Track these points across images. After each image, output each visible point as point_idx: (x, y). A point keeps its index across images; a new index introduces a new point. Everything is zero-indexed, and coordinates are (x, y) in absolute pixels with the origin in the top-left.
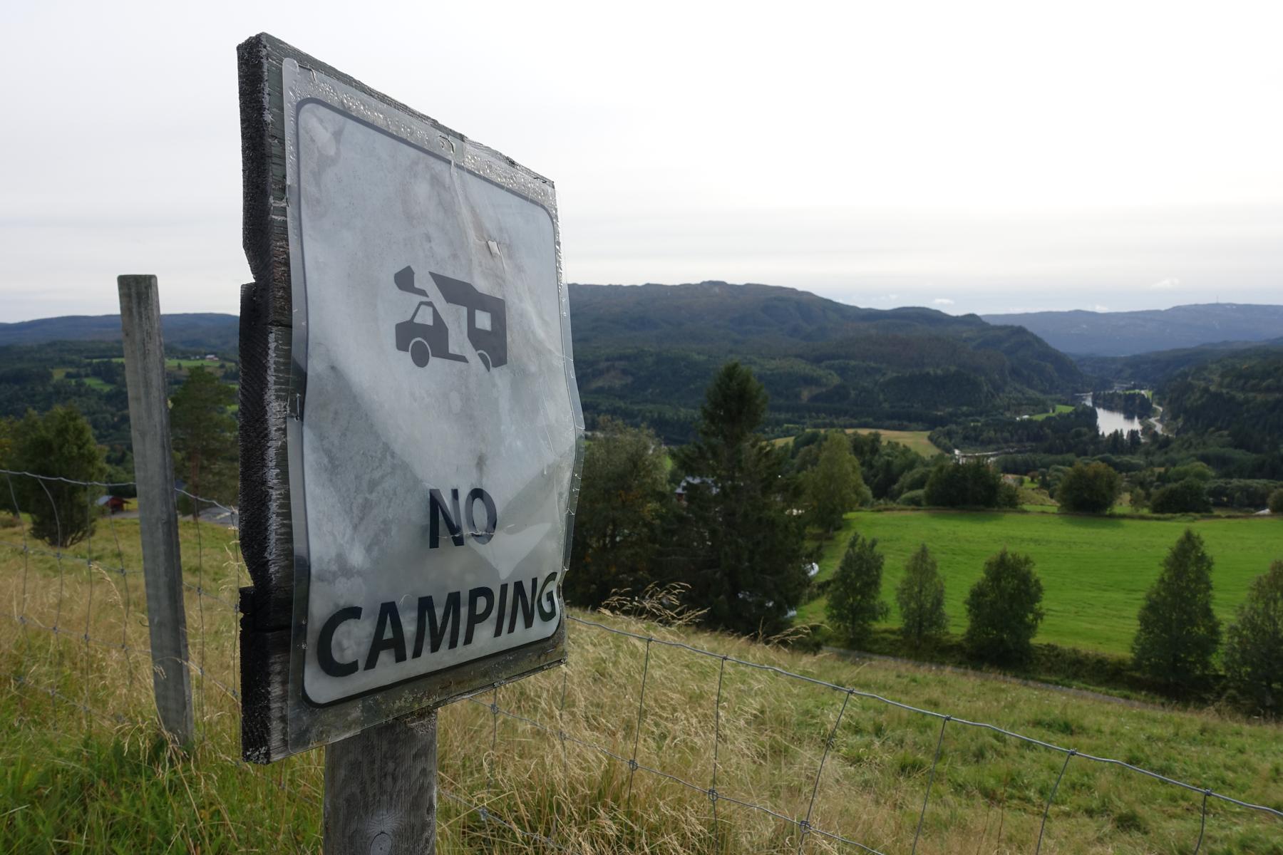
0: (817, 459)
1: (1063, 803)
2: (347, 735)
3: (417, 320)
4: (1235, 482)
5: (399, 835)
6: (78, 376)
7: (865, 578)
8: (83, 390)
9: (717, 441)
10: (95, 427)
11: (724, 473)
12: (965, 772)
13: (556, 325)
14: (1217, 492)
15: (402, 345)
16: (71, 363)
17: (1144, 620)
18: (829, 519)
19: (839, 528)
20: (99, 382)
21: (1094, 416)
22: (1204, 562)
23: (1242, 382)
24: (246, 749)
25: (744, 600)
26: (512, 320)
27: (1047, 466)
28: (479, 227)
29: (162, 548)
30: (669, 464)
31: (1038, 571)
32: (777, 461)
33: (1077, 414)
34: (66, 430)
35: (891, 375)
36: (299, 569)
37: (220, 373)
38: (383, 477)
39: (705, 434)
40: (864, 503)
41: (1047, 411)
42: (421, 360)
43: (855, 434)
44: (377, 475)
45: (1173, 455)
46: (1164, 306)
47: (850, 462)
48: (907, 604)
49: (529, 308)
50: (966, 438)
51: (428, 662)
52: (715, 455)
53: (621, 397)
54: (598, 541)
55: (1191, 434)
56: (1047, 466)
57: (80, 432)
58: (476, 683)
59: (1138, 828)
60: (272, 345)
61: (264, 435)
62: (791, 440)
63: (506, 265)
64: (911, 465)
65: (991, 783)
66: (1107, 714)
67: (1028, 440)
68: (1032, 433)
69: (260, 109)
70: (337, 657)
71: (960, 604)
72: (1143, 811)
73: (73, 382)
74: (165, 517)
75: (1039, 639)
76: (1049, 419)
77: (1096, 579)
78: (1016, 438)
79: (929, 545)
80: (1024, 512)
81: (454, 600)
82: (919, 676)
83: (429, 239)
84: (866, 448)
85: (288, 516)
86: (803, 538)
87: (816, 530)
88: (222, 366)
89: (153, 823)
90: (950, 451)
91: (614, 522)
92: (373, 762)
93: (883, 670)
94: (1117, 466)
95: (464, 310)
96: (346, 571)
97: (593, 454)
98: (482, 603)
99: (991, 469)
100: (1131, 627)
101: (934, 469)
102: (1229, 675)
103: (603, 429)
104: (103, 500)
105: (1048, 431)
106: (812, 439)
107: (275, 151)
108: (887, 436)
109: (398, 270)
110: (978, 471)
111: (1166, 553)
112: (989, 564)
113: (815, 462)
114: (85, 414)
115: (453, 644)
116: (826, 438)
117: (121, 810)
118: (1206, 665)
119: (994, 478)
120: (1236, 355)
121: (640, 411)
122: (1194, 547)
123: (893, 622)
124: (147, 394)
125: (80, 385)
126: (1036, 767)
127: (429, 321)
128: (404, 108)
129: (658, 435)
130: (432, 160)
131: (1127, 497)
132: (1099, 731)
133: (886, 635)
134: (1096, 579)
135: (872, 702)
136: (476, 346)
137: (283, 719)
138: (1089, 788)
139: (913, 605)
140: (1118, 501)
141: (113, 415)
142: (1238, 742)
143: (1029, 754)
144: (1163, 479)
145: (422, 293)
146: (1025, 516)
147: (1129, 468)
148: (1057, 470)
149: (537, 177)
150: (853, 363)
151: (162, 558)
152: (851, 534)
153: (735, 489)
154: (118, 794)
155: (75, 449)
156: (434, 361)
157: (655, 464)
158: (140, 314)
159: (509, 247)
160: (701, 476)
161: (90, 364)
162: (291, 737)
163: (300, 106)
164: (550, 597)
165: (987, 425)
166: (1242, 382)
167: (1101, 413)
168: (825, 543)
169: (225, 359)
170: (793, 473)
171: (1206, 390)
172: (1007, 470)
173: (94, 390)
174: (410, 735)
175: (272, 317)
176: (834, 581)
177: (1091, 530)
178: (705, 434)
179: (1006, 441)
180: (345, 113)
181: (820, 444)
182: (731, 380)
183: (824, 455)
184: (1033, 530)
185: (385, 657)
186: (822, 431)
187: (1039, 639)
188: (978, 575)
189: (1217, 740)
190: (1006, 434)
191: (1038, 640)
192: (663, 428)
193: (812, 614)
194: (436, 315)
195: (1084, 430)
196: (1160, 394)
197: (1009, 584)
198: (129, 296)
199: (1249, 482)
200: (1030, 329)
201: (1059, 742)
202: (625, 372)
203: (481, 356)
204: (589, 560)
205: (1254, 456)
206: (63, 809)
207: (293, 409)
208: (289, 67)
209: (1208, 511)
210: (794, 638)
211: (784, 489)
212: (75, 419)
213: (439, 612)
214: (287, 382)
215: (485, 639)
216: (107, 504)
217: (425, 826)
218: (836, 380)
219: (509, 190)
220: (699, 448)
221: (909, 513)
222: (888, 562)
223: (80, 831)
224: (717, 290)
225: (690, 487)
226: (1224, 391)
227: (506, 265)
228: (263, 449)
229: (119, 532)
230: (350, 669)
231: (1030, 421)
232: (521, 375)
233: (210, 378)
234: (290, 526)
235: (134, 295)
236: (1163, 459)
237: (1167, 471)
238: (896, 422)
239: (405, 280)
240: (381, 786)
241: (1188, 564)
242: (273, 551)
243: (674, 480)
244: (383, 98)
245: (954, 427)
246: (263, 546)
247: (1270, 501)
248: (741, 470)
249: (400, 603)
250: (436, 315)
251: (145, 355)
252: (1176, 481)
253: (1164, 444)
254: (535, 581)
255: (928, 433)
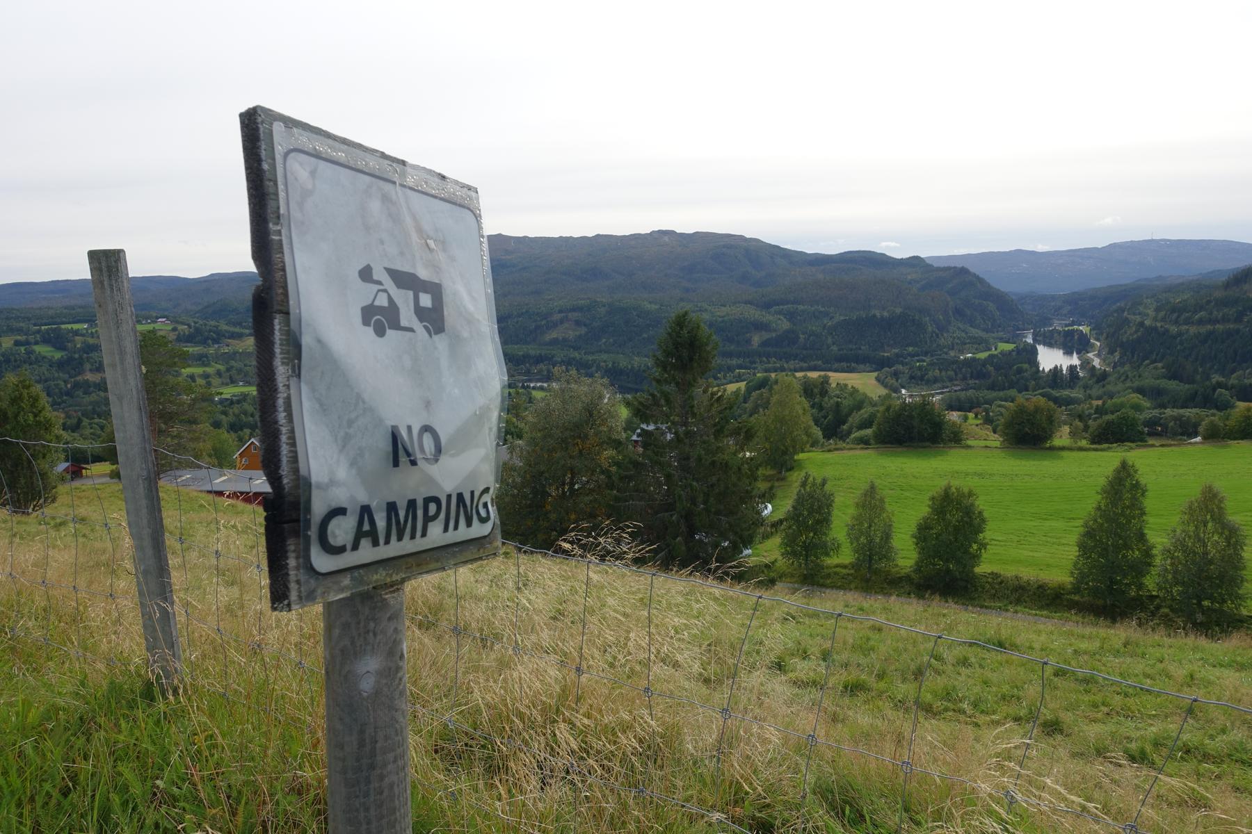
0: (768, 402)
1: (994, 713)
2: (341, 596)
3: (377, 303)
4: (1169, 412)
5: (380, 674)
6: (27, 343)
7: (817, 516)
8: (33, 357)
9: (670, 388)
10: (48, 395)
11: (677, 419)
12: (904, 689)
13: (482, 301)
14: (1152, 423)
15: (366, 322)
16: (19, 331)
17: (1082, 546)
18: (781, 460)
19: (791, 469)
20: (50, 349)
21: (1035, 352)
22: (1138, 489)
23: (1175, 315)
24: (273, 603)
25: (700, 541)
26: (447, 299)
27: (990, 402)
28: (420, 230)
29: (144, 502)
30: (624, 413)
31: (981, 504)
32: (729, 407)
33: (1018, 351)
34: (20, 398)
35: (839, 318)
36: (304, 484)
37: (172, 336)
38: (357, 417)
39: (658, 381)
40: (814, 444)
41: (990, 349)
42: (380, 332)
43: (805, 377)
44: (353, 416)
45: (1110, 388)
46: (1101, 243)
47: (800, 406)
48: (857, 539)
49: (461, 289)
50: (912, 378)
51: (396, 548)
52: (668, 401)
53: (576, 348)
54: (557, 489)
55: (1127, 367)
56: (990, 402)
57: (36, 399)
58: (432, 566)
59: (1061, 732)
60: (277, 327)
61: (274, 390)
62: (742, 385)
63: (441, 256)
64: (859, 406)
65: (928, 697)
66: (1039, 632)
67: (972, 377)
68: (976, 371)
69: (259, 161)
70: (331, 541)
71: (907, 537)
72: (1067, 717)
73: (23, 349)
74: (145, 473)
75: (983, 568)
76: (991, 356)
77: (1036, 509)
78: (960, 376)
79: (877, 482)
80: (969, 447)
81: (412, 504)
82: (866, 605)
83: (382, 242)
84: (816, 390)
85: (294, 444)
86: (756, 480)
87: (769, 472)
88: (174, 329)
89: (151, 748)
90: (897, 391)
91: (572, 470)
92: (359, 623)
93: (832, 602)
94: (1056, 400)
95: (411, 293)
96: (332, 482)
97: (548, 404)
98: (433, 508)
99: (937, 406)
100: (1071, 553)
101: (882, 409)
102: (1161, 595)
103: (558, 380)
104: (62, 466)
105: (991, 368)
106: (763, 384)
107: (271, 190)
108: (836, 378)
109: (361, 267)
110: (924, 409)
111: (1102, 481)
112: (933, 499)
113: (766, 405)
114: (38, 382)
115: (413, 537)
116: (776, 382)
117: (121, 738)
118: (1140, 586)
119: (939, 416)
120: (1170, 289)
121: (594, 361)
122: (1129, 475)
123: (846, 556)
124: (122, 361)
125: (29, 353)
126: (971, 682)
127: (385, 304)
128: (360, 146)
129: (612, 385)
130: (381, 183)
131: (1066, 429)
132: (1031, 648)
133: (838, 570)
134: (1036, 509)
135: (820, 630)
136: (421, 320)
137: (298, 582)
138: (1019, 698)
139: (863, 540)
140: (1058, 434)
141: (66, 382)
142: (1157, 653)
143: (963, 670)
144: (1100, 411)
145: (380, 283)
146: (969, 451)
147: (1069, 402)
148: (1000, 406)
149: (464, 186)
150: (801, 307)
151: (144, 511)
152: (803, 474)
153: (688, 434)
154: (117, 725)
155: (31, 417)
156: (390, 333)
157: (609, 412)
158: (111, 286)
159: (443, 242)
160: (656, 423)
161: (39, 332)
162: (304, 594)
163: (286, 155)
164: (485, 505)
165: (932, 364)
166: (1175, 315)
167: (1041, 349)
168: (776, 484)
169: (177, 322)
170: (745, 417)
171: (1142, 324)
172: (951, 408)
173: (44, 357)
174: (385, 604)
175: (276, 307)
176: (786, 520)
177: (1032, 463)
178: (658, 381)
179: (951, 380)
180: (317, 156)
181: (771, 389)
182: (681, 328)
183: (774, 399)
184: (978, 465)
185: (365, 543)
186: (773, 375)
187: (983, 568)
188: (921, 510)
189: (1140, 651)
190: (951, 373)
191: (982, 569)
192: (617, 377)
193: (767, 551)
194: (390, 299)
195: (1026, 366)
196: (1097, 328)
197: (954, 517)
198: (101, 270)
199: (1182, 411)
200: (972, 270)
201: (993, 657)
202: (578, 323)
203: (425, 327)
204: (549, 507)
205: (1187, 386)
206: (68, 740)
207: (294, 371)
208: (278, 127)
209: (1142, 440)
210: (737, 570)
211: (736, 432)
212: (28, 387)
213: (402, 514)
214: (288, 353)
215: (436, 534)
216: (66, 470)
217: (398, 669)
218: (785, 325)
219: (442, 199)
220: (653, 395)
221: (858, 452)
222: (838, 500)
223: (86, 758)
224: (666, 239)
225: (645, 433)
226: (1159, 325)
227: (441, 256)
228: (275, 399)
229: (80, 498)
230: (341, 550)
231: (973, 359)
232: (456, 342)
233: (163, 342)
234: (296, 452)
235: (105, 269)
236: (1100, 392)
237: (1104, 404)
238: (844, 364)
239: (366, 274)
240: (365, 639)
241: (1123, 492)
242: (285, 469)
243: (629, 427)
244: (344, 141)
245: (900, 367)
246: (277, 465)
247: (1201, 429)
248: (694, 415)
249: (374, 505)
250: (390, 299)
251: (118, 324)
252: (1112, 413)
253: (1102, 377)
254: (472, 493)
255: (875, 374)
